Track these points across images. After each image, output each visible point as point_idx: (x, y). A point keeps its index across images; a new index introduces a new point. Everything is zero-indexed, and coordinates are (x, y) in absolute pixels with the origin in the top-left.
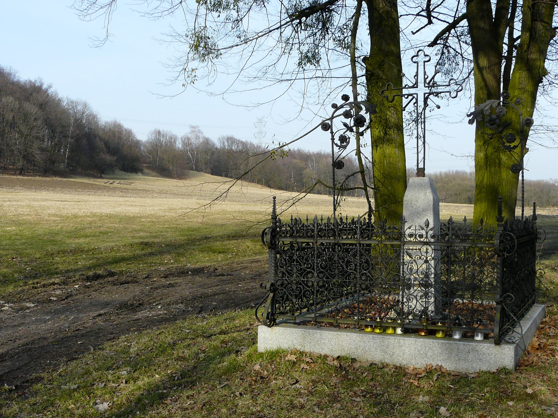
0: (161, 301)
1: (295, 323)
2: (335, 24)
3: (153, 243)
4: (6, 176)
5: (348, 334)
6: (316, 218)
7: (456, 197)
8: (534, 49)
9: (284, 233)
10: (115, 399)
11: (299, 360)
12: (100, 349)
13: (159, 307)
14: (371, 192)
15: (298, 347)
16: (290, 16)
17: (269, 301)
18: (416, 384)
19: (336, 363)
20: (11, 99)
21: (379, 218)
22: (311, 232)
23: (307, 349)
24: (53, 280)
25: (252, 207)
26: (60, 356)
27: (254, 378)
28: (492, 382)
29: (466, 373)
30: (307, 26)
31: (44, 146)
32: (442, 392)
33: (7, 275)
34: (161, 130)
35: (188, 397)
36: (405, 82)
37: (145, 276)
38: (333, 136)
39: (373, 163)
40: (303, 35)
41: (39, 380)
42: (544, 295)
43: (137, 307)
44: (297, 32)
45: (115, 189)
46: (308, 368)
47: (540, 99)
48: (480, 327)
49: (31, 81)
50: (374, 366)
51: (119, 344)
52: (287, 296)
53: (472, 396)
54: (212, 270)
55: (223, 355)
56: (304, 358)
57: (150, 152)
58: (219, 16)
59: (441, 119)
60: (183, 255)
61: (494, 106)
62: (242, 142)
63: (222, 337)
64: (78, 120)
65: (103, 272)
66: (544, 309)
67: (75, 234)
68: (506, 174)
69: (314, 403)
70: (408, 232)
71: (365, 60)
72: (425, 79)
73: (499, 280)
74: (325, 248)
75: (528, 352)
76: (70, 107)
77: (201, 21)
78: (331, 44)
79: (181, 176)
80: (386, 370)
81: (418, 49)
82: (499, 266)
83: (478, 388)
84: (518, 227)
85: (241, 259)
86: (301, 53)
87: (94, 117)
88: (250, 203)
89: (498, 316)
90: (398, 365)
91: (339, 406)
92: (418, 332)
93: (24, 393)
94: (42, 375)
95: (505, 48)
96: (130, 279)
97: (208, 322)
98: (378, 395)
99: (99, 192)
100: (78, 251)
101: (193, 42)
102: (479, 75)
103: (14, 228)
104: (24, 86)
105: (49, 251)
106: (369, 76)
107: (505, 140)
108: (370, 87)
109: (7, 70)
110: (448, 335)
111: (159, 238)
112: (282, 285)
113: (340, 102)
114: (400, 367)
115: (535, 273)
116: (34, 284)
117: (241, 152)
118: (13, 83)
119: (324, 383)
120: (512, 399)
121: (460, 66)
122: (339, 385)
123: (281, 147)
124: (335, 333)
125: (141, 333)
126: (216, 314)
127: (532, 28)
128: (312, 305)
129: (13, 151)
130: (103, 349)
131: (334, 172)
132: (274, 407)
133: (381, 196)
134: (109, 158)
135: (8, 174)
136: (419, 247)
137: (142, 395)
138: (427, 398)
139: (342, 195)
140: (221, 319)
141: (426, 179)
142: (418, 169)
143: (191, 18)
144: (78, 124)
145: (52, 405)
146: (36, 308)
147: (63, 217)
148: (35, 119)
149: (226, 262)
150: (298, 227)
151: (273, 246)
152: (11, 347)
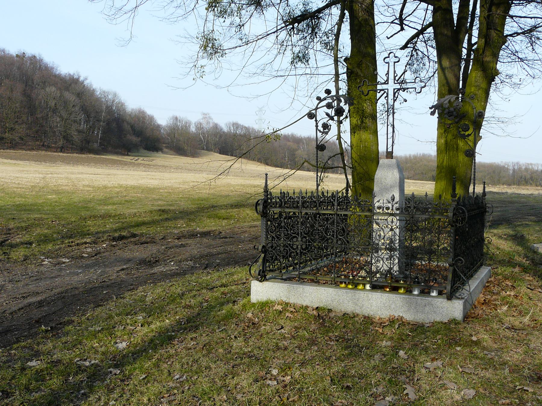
0: (174, 259)
1: (282, 279)
2: (323, 29)
3: (169, 210)
4: (49, 153)
5: (326, 288)
6: (301, 192)
7: (421, 176)
8: (488, 53)
9: (274, 204)
10: (132, 340)
11: (285, 309)
12: (121, 298)
13: (172, 263)
14: (349, 171)
15: (284, 299)
16: (284, 22)
17: (261, 260)
18: (381, 331)
19: (315, 312)
20: (53, 89)
21: (355, 192)
22: (296, 204)
23: (292, 301)
24: (85, 240)
25: (252, 181)
26: (88, 303)
27: (247, 324)
28: (443, 330)
29: (422, 323)
30: (299, 30)
31: (81, 128)
32: (402, 338)
33: (47, 235)
34: (178, 117)
35: (192, 339)
36: (379, 79)
37: (161, 237)
38: (317, 124)
39: (351, 147)
40: (295, 38)
41: (71, 322)
42: (491, 259)
43: (154, 263)
44: (290, 36)
45: (139, 165)
46: (292, 316)
47: (493, 95)
48: (435, 285)
49: (70, 74)
50: (346, 315)
51: (137, 294)
52: (276, 257)
53: (427, 342)
54: (217, 233)
55: (222, 304)
56: (289, 308)
57: (169, 135)
58: (224, 21)
59: (409, 110)
60: (193, 220)
61: (452, 100)
62: (245, 127)
63: (222, 289)
65: (126, 234)
66: (490, 271)
67: (105, 202)
68: (462, 158)
69: (296, 345)
70: (377, 205)
71: (346, 60)
72: (395, 77)
73: (452, 246)
74: (309, 217)
75: (475, 306)
76: (103, 96)
77: (209, 25)
78: (319, 46)
79: (194, 155)
80: (356, 319)
81: (389, 52)
82: (452, 235)
83: (432, 336)
84: (469, 202)
85: (242, 224)
86: (294, 53)
87: (123, 104)
88: (247, 178)
89: (450, 276)
91: (316, 348)
92: (383, 288)
94: (73, 318)
95: (465, 52)
96: (149, 240)
97: (212, 277)
98: (349, 340)
99: (126, 167)
100: (106, 216)
101: (202, 43)
102: (442, 75)
103: (54, 196)
104: (64, 78)
105: (82, 216)
106: (350, 73)
107: (460, 130)
108: (350, 83)
109: (50, 65)
110: (409, 291)
111: (174, 206)
112: (272, 247)
113: (323, 95)
114: (368, 317)
115: (483, 240)
116: (69, 243)
117: (244, 136)
119: (305, 329)
120: (460, 345)
121: (427, 67)
122: (317, 331)
123: (275, 132)
124: (315, 288)
125: (156, 285)
126: (219, 270)
127: (487, 35)
128: (296, 264)
129: (55, 132)
130: (124, 298)
131: (317, 154)
132: (262, 348)
133: (357, 174)
134: (135, 139)
135: (51, 151)
137: (155, 336)
138: (389, 343)
139: (325, 172)
140: (222, 274)
141: (394, 161)
142: (387, 152)
143: (201, 23)
144: (109, 110)
145: (80, 343)
146: (70, 263)
147: (95, 187)
149: (229, 227)
150: (285, 199)
151: (264, 215)
152: (48, 295)
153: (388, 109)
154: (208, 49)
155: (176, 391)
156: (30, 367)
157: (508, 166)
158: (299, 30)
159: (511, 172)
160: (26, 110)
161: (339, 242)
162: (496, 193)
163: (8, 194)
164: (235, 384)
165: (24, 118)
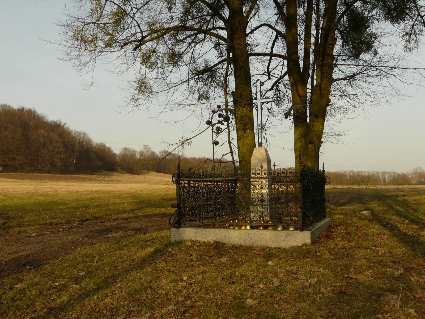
4: (40, 174)
11: (193, 244)
20: (43, 131)
30: (203, 79)
46: (198, 248)
48: (292, 223)
49: (54, 121)
53: (287, 257)
71: (232, 93)
87: (90, 141)
93: (38, 270)
109: (41, 115)
129: (44, 160)
134: (98, 163)
136: (258, 180)
144: (81, 144)
153: (262, 127)
154: (142, 89)
155: (117, 292)
156: (16, 288)
157: (346, 173)
158: (203, 79)
159: (348, 177)
162: (339, 188)
163: (9, 197)
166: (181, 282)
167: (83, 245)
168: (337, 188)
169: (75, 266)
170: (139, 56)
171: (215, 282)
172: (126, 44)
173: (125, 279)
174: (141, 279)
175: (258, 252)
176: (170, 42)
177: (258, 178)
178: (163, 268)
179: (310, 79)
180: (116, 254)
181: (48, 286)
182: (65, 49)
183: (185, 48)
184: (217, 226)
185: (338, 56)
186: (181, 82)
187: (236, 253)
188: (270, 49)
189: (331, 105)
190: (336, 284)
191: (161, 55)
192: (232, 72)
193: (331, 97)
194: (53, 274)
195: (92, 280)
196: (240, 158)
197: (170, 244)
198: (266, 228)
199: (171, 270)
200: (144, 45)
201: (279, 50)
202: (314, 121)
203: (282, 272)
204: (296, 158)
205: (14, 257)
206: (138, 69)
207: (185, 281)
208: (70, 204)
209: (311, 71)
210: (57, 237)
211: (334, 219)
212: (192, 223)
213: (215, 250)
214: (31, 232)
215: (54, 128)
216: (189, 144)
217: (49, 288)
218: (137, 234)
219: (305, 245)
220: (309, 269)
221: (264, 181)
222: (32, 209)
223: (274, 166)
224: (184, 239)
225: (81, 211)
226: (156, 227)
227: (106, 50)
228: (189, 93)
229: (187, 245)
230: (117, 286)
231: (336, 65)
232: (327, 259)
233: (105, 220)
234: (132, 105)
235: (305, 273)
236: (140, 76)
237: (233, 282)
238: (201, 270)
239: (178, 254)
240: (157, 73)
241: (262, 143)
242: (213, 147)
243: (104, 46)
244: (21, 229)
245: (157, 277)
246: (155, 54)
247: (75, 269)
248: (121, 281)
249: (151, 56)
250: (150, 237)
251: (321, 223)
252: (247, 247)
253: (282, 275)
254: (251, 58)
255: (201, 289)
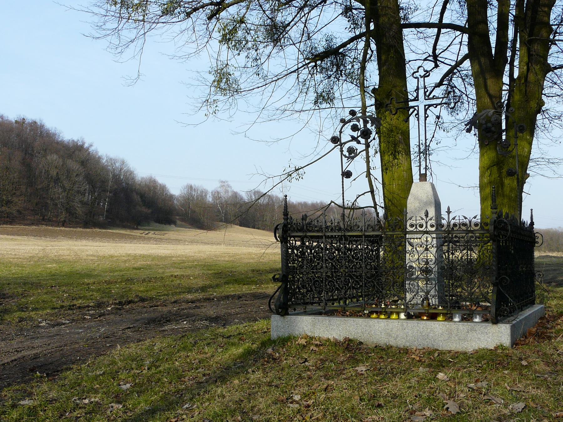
4: (50, 228)
11: (309, 343)
20: (55, 157)
30: (323, 68)
34: (193, 185)
46: (317, 349)
48: (478, 309)
49: (73, 141)
53: (470, 367)
57: (183, 205)
64: (116, 176)
71: (374, 91)
86: (317, 93)
87: (131, 173)
90: (402, 347)
92: (420, 317)
93: (54, 379)
103: (54, 265)
109: (53, 131)
118: (58, 143)
129: (56, 205)
134: (145, 210)
136: (419, 236)
144: (116, 178)
148: (77, 175)
154: (222, 84)
155: (184, 416)
156: (23, 405)
160: (25, 181)
161: (368, 267)
162: (554, 257)
164: (252, 407)
165: (23, 188)
166: (291, 403)
167: (125, 341)
168: (551, 257)
169: (114, 375)
170: (216, 29)
171: (348, 404)
172: (195, 10)
173: (197, 397)
174: (224, 397)
175: (420, 357)
176: (268, 6)
177: (420, 232)
178: (259, 380)
179: (507, 67)
180: (180, 357)
181: (72, 405)
182: (96, 19)
183: (294, 14)
184: (348, 313)
185: (559, 25)
186: (285, 73)
187: (382, 358)
188: (439, 16)
189: (543, 111)
190: (558, 414)
191: (252, 28)
192: (371, 56)
193: (544, 97)
194: (79, 385)
195: (142, 398)
196: (387, 201)
197: (270, 342)
198: (433, 317)
199: (273, 384)
200: (224, 11)
201: (453, 19)
202: (516, 137)
203: (462, 391)
204: (483, 200)
205: (16, 357)
206: (215, 51)
207: (297, 402)
208: (100, 276)
209: (509, 54)
210: (81, 328)
211: (549, 307)
212: (308, 307)
213: (346, 352)
214: (40, 320)
215: (74, 152)
216: (300, 177)
217: (74, 408)
218: (212, 326)
219: (501, 347)
220: (509, 388)
221: (429, 239)
222: (40, 283)
223: (449, 212)
224: (294, 334)
225: (117, 288)
226: (243, 315)
227: (163, 19)
228: (298, 92)
229: (298, 344)
230: (185, 406)
231: (554, 42)
232: (539, 373)
233: (159, 303)
234: (206, 112)
235: (502, 394)
236: (219, 63)
237: (379, 406)
238: (323, 384)
239: (283, 358)
240: (247, 57)
241: (426, 174)
242: (343, 182)
243: (160, 13)
244: (24, 315)
245: (250, 395)
246: (244, 25)
247: (114, 379)
248: (191, 399)
249: (236, 30)
250: (235, 331)
251: (528, 312)
252: (400, 349)
253: (462, 395)
254: (405, 31)
255: (324, 415)
